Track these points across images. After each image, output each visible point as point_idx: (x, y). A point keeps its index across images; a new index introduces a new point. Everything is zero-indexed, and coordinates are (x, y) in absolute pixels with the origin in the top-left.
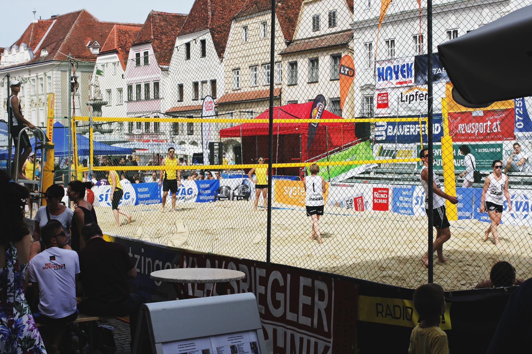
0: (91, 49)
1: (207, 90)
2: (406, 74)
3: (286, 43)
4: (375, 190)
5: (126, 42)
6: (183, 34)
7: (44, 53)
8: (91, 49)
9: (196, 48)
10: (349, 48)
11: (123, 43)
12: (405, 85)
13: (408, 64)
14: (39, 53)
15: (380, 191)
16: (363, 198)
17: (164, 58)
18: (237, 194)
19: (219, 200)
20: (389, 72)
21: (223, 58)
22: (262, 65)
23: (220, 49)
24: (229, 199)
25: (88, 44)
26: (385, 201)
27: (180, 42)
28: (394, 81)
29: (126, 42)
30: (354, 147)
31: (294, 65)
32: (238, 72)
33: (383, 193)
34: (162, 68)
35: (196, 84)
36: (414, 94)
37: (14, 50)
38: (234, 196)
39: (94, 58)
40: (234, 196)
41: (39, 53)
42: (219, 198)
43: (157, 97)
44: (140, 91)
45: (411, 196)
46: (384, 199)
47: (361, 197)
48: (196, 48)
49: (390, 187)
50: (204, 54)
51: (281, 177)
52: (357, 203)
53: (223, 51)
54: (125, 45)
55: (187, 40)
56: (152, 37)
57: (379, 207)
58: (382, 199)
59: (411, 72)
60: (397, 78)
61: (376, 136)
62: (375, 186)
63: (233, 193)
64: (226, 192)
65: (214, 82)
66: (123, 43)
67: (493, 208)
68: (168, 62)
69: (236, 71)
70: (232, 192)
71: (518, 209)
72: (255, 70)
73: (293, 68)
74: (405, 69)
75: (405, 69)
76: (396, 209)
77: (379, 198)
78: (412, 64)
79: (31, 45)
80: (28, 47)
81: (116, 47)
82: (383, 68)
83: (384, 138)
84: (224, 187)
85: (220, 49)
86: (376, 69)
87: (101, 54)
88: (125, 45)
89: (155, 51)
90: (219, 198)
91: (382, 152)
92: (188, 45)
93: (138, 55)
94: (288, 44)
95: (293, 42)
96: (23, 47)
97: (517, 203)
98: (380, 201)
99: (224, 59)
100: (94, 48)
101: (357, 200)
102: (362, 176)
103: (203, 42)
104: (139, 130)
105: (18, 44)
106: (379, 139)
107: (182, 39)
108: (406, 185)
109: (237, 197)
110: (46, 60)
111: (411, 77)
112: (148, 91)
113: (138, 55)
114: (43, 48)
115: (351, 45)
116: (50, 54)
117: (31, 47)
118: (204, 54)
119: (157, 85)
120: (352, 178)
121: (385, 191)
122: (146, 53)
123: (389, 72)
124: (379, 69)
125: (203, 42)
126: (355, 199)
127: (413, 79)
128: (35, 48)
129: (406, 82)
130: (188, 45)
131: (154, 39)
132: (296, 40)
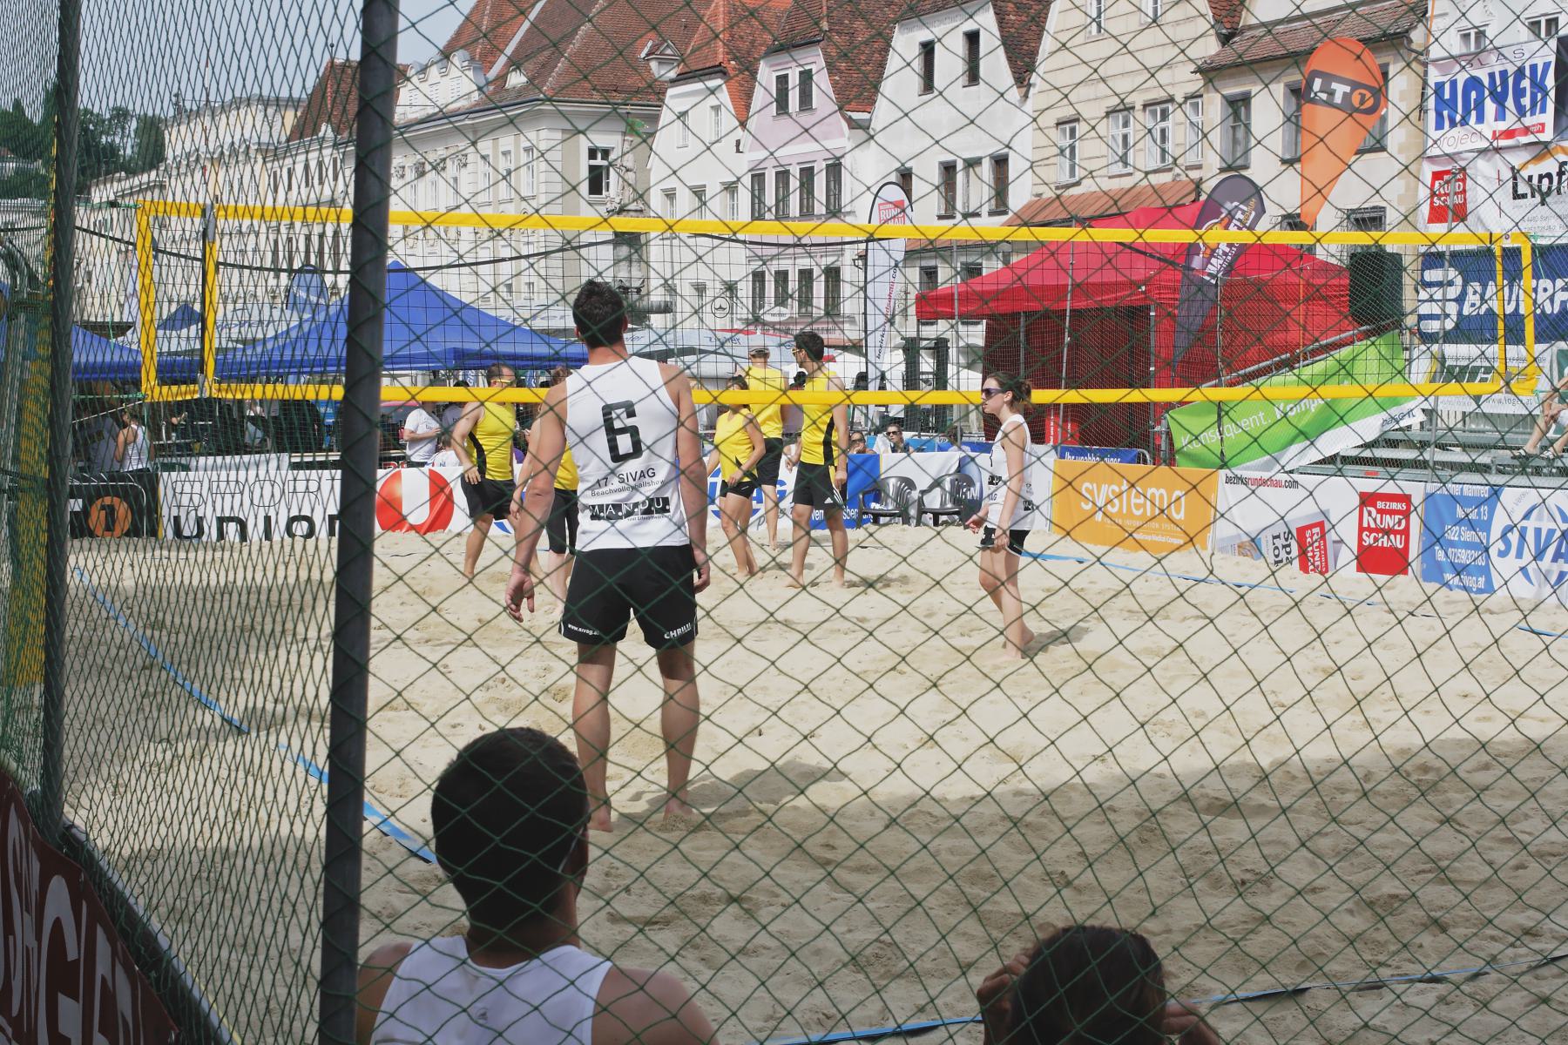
0: (654, 65)
1: (976, 190)
2: (1526, 101)
3: (1218, 35)
4: (1367, 499)
5: (753, 42)
6: (914, 13)
7: (516, 79)
8: (654, 65)
9: (949, 63)
10: (1414, 46)
11: (744, 46)
12: (1524, 140)
13: (1534, 68)
14: (502, 77)
15: (1380, 505)
16: (1327, 526)
17: (858, 89)
18: (936, 505)
19: (876, 522)
20: (1473, 95)
21: (1029, 85)
22: (1145, 106)
23: (1023, 65)
24: (906, 521)
25: (646, 50)
26: (1398, 542)
27: (906, 42)
28: (1491, 125)
29: (753, 42)
30: (1345, 352)
31: (1238, 106)
32: (1073, 131)
33: (1392, 512)
34: (850, 121)
35: (949, 169)
36: (1554, 172)
37: (434, 71)
38: (922, 511)
39: (656, 92)
40: (922, 511)
41: (502, 77)
42: (876, 517)
43: (834, 211)
44: (762, 189)
45: (1487, 526)
46: (1396, 532)
47: (1321, 525)
48: (949, 63)
49: (1416, 489)
50: (973, 76)
51: (1090, 451)
52: (1308, 545)
53: (1031, 68)
54: (748, 53)
55: (924, 35)
56: (825, 26)
57: (1380, 560)
58: (1388, 532)
59: (1546, 94)
60: (1500, 116)
61: (1421, 318)
62: (1370, 485)
63: (921, 502)
64: (899, 492)
65: (1000, 162)
66: (744, 46)
67: (934, 501)
68: (869, 103)
69: (1067, 127)
70: (915, 495)
71: (1538, 556)
72: (1126, 124)
73: (1236, 115)
74: (1526, 83)
75: (1526, 83)
76: (1433, 572)
77: (1377, 530)
78: (1546, 66)
79: (483, 56)
80: (472, 59)
81: (720, 58)
82: (1454, 84)
83: (1449, 325)
84: (892, 482)
85: (1023, 65)
86: (1430, 91)
87: (682, 78)
88: (748, 53)
89: (831, 68)
90: (876, 517)
91: (1450, 373)
92: (928, 49)
93: (782, 80)
94: (1225, 40)
95: (1242, 32)
96: (458, 58)
97: (1538, 531)
98: (1384, 542)
99: (1032, 90)
100: (661, 62)
101: (1308, 533)
102: (1367, 454)
103: (973, 38)
104: (783, 310)
105: (446, 54)
106: (1433, 326)
107: (911, 30)
108: (1470, 486)
109: (936, 515)
110: (520, 98)
111: (1543, 110)
112: (810, 192)
113: (782, 80)
114: (515, 63)
115: (1417, 36)
116: (531, 80)
117: (482, 62)
118: (973, 76)
119: (834, 169)
120: (1331, 460)
121: (1395, 506)
122: (806, 77)
123: (1473, 95)
124: (1439, 87)
125: (973, 38)
126: (1302, 531)
127: (1548, 118)
128: (493, 63)
129: (1527, 130)
130: (928, 49)
131: (830, 30)
132: (1251, 27)
